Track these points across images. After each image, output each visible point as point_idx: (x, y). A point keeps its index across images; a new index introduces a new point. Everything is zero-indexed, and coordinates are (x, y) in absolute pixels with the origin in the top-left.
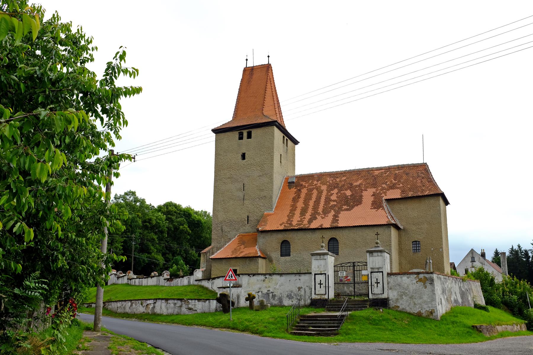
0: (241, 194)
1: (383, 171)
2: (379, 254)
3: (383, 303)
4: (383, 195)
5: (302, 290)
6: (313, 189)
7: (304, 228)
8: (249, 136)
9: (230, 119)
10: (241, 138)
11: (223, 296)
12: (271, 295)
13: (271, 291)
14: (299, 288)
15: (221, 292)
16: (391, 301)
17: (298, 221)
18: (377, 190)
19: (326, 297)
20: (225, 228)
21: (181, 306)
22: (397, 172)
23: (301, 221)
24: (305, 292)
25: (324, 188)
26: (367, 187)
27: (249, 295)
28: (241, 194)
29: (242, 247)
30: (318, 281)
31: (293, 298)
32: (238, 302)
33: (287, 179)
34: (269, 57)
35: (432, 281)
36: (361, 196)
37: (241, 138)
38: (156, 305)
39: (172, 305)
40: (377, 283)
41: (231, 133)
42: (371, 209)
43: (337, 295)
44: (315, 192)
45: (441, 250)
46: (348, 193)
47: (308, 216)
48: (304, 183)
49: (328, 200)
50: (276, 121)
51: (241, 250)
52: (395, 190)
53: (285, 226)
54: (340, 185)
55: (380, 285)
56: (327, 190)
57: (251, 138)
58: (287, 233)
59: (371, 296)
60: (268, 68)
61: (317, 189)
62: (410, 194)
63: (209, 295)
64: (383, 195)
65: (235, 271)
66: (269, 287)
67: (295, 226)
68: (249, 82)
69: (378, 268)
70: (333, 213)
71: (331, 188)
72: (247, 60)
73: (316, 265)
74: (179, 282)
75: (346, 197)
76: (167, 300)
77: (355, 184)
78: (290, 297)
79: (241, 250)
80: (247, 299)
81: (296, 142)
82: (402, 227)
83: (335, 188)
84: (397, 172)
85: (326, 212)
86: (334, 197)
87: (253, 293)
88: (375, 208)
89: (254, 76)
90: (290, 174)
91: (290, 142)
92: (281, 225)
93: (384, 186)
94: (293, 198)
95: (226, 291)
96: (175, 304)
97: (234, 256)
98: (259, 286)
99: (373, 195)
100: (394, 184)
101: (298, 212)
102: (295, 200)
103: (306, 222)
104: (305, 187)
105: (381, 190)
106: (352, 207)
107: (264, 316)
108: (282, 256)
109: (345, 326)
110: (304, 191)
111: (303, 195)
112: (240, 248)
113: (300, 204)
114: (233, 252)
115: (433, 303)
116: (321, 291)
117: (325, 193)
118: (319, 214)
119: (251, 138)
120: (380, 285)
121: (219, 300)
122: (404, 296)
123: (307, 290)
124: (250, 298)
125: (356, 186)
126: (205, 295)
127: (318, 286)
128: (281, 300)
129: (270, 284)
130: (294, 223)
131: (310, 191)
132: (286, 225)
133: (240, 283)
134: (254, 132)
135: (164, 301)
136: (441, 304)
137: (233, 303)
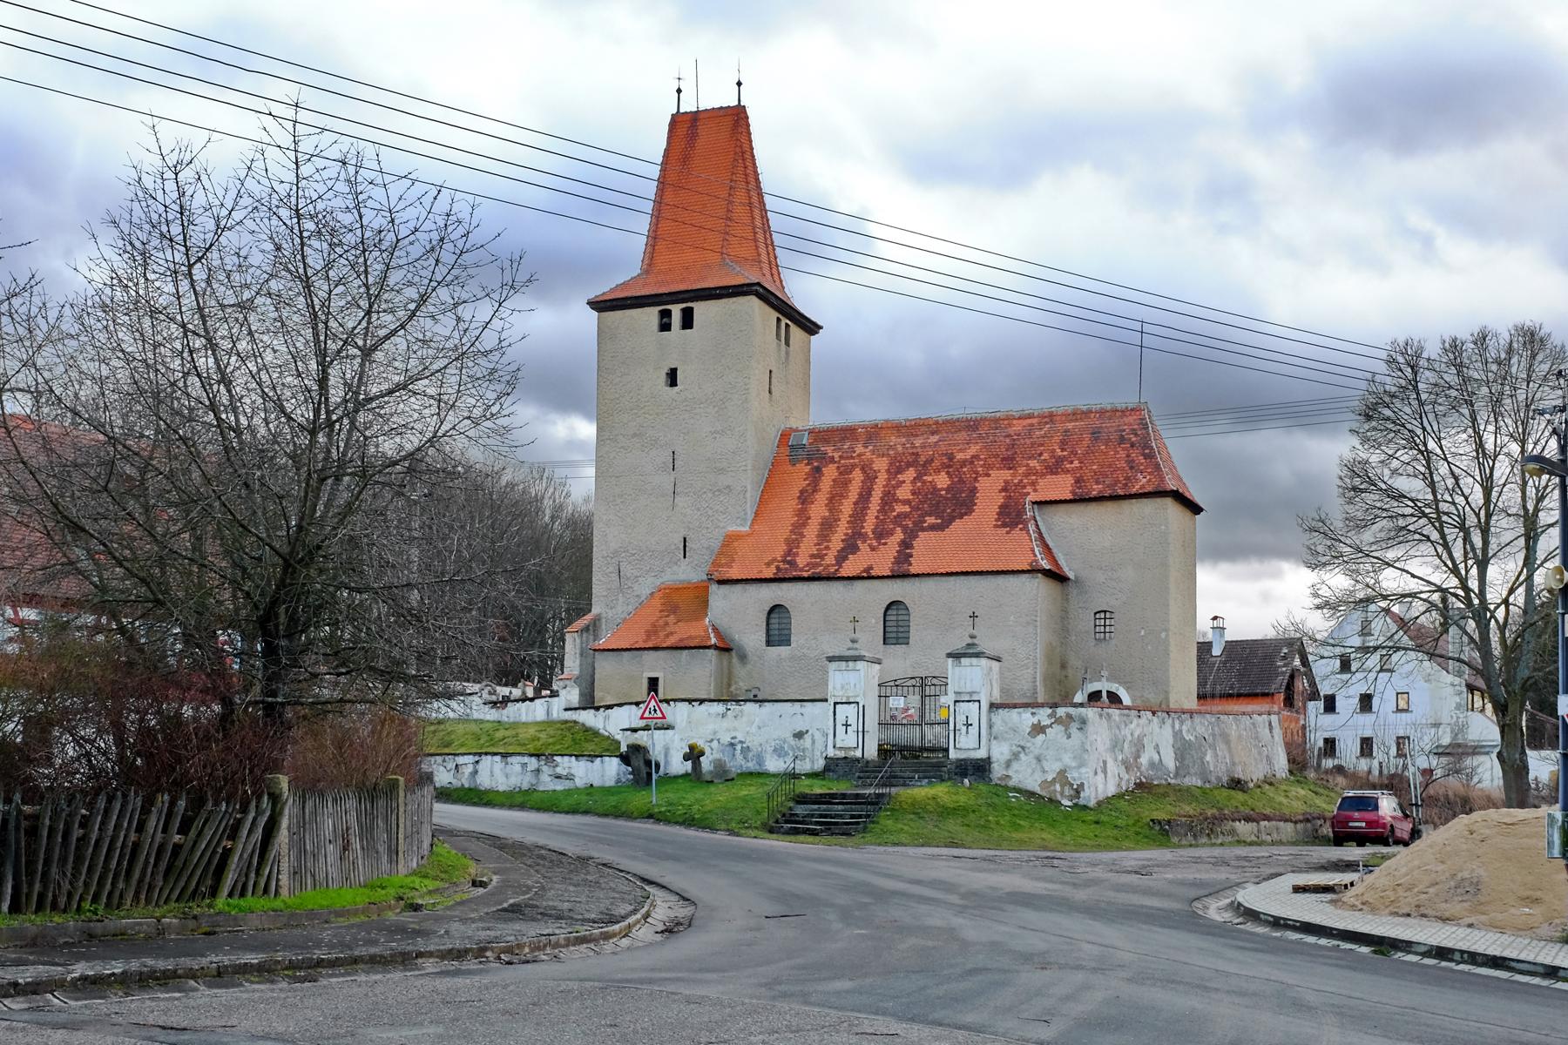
0: (666, 480)
1: (1035, 421)
2: (974, 661)
3: (979, 769)
4: (1029, 489)
5: (807, 740)
6: (854, 466)
7: (824, 574)
8: (688, 322)
9: (636, 270)
10: (665, 327)
11: (636, 749)
12: (739, 747)
13: (740, 737)
14: (799, 735)
15: (630, 741)
16: (995, 766)
17: (812, 556)
18: (1014, 475)
19: (858, 754)
20: (627, 570)
21: (538, 770)
22: (1070, 426)
23: (822, 557)
24: (814, 742)
25: (881, 465)
26: (990, 467)
27: (692, 748)
28: (666, 480)
29: (672, 619)
30: (840, 719)
31: (786, 754)
32: (667, 762)
33: (785, 436)
34: (739, 84)
35: (1084, 722)
36: (974, 491)
37: (665, 327)
38: (480, 767)
39: (518, 768)
40: (968, 725)
41: (639, 310)
42: (996, 526)
43: (883, 751)
44: (857, 476)
45: (1163, 635)
46: (942, 481)
47: (836, 543)
48: (829, 450)
49: (889, 499)
50: (759, 284)
51: (668, 629)
52: (1060, 478)
53: (778, 568)
54: (922, 459)
55: (974, 730)
56: (888, 471)
57: (691, 327)
58: (785, 586)
59: (953, 755)
60: (736, 117)
61: (863, 469)
62: (1096, 490)
63: (589, 744)
64: (1029, 489)
65: (653, 683)
66: (735, 729)
67: (802, 570)
68: (685, 159)
69: (971, 694)
70: (899, 535)
71: (896, 469)
72: (679, 91)
73: (841, 681)
74: (523, 711)
75: (935, 490)
76: (505, 755)
77: (960, 456)
78: (779, 752)
79: (668, 629)
80: (686, 757)
81: (811, 328)
82: (1071, 575)
83: (909, 465)
84: (1070, 426)
85: (881, 534)
86: (904, 493)
87: (701, 743)
88: (1004, 525)
89: (701, 142)
90: (794, 424)
91: (796, 332)
92: (768, 564)
93: (1033, 463)
94: (801, 492)
95: (642, 738)
96: (524, 765)
97: (650, 645)
98: (711, 727)
99: (1004, 490)
100: (1060, 461)
101: (811, 531)
102: (805, 498)
103: (830, 559)
104: (832, 460)
105: (1027, 475)
106: (952, 520)
107: (720, 796)
108: (769, 643)
109: (885, 821)
110: (830, 472)
111: (826, 484)
112: (667, 624)
113: (818, 510)
114: (649, 634)
115: (1083, 770)
116: (848, 740)
117: (882, 479)
118: (864, 537)
119: (691, 327)
120: (974, 730)
121: (625, 759)
122: (1022, 755)
123: (818, 736)
124: (694, 755)
125: (963, 463)
126: (589, 744)
127: (840, 729)
128: (760, 759)
129: (736, 723)
130: (801, 561)
131: (845, 471)
132: (782, 565)
133: (669, 719)
134: (701, 309)
135: (498, 758)
136: (1105, 772)
137: (658, 766)
